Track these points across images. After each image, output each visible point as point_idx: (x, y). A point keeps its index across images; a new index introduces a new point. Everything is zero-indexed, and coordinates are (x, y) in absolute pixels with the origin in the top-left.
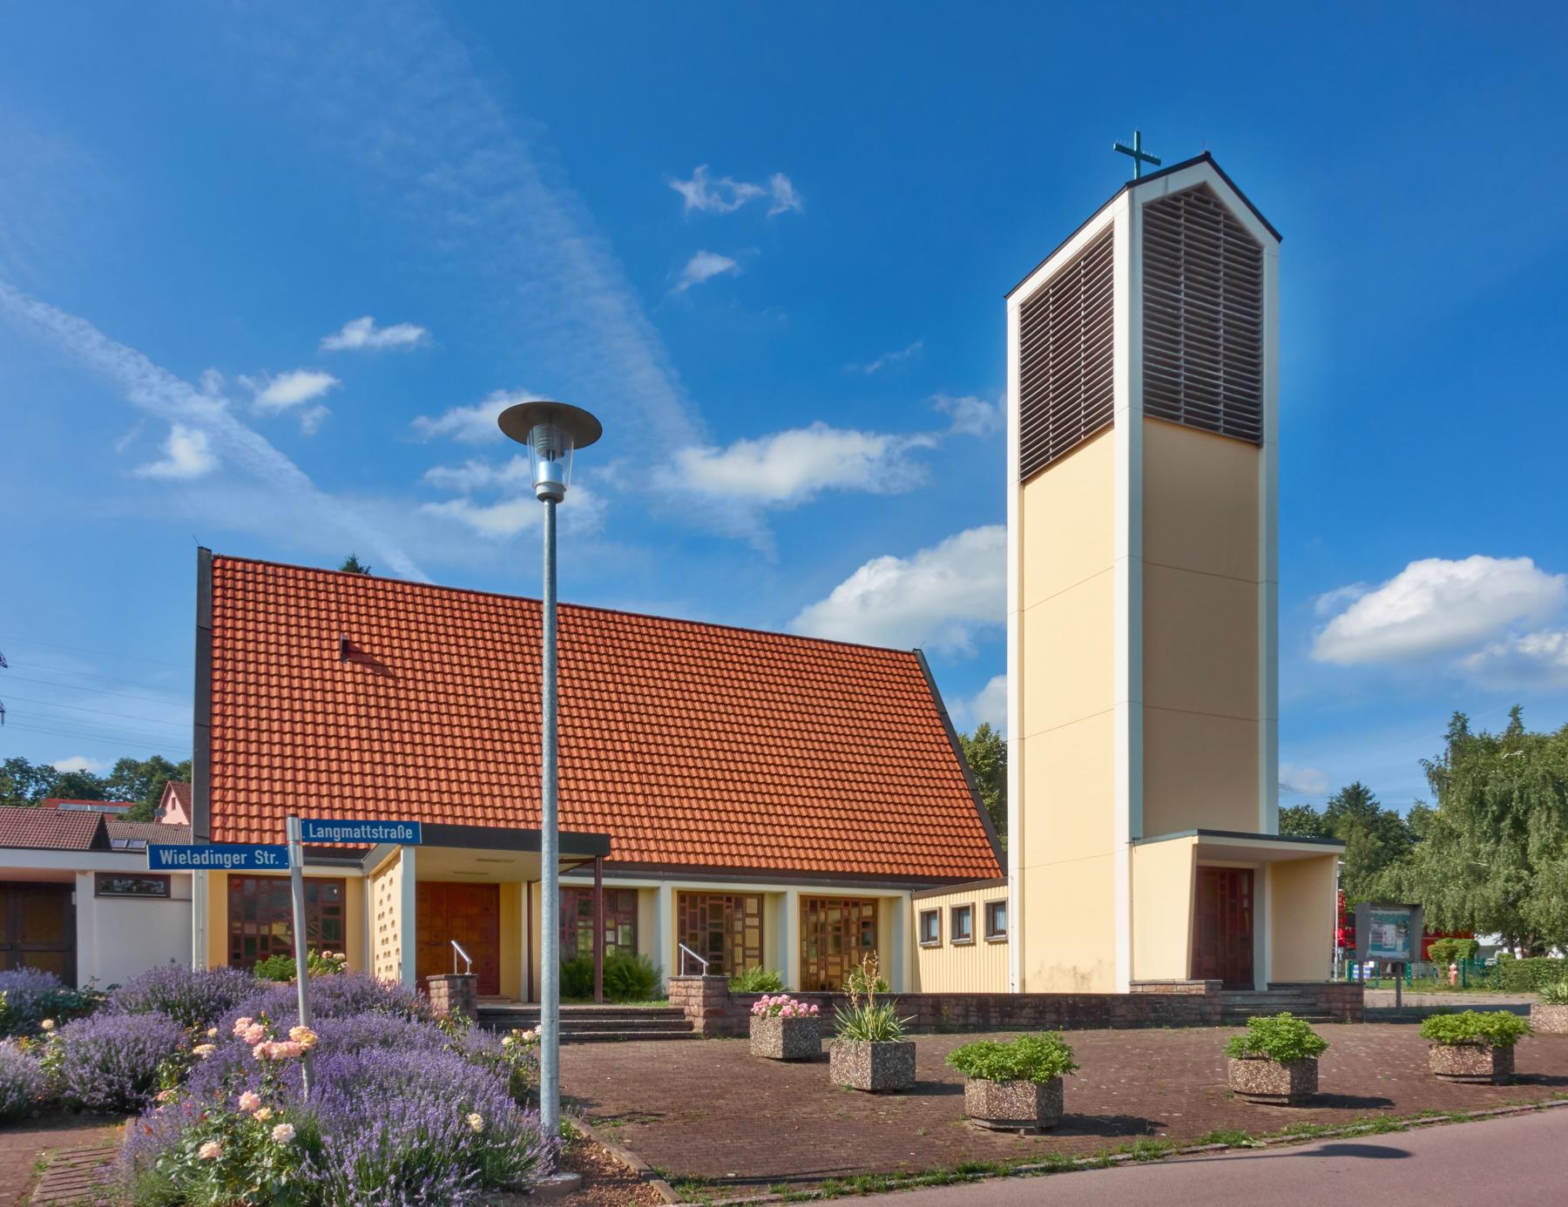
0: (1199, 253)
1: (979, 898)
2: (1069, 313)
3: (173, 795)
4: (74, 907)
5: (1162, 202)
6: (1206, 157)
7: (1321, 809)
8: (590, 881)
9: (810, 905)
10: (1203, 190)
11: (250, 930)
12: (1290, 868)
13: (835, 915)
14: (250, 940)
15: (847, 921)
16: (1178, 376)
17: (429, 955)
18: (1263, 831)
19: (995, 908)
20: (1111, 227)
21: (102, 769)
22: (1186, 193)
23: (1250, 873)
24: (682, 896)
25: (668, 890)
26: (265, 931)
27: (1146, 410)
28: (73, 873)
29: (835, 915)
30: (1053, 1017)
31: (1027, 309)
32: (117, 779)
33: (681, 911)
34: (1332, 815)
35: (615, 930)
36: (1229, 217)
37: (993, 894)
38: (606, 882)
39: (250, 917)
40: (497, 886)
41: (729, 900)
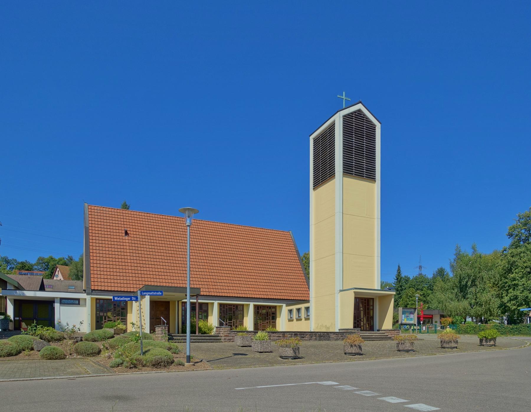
0: (358, 131)
1: (303, 306)
2: (325, 142)
3: (58, 269)
4: (54, 308)
5: (348, 115)
6: (361, 102)
7: (430, 276)
8: (195, 301)
9: (257, 308)
10: (359, 110)
11: (101, 314)
12: (382, 298)
13: (264, 311)
14: (101, 317)
15: (511, 300)
16: (352, 162)
17: (155, 322)
18: (376, 288)
19: (307, 309)
20: (334, 121)
21: (33, 261)
22: (355, 112)
23: (373, 299)
24: (221, 305)
25: (216, 303)
26: (105, 314)
27: (344, 172)
28: (54, 298)
29: (264, 311)
30: (315, 338)
31: (316, 141)
32: (38, 263)
33: (220, 309)
34: (434, 277)
35: (202, 315)
36: (367, 118)
37: (306, 305)
38: (199, 301)
39: (101, 311)
40: (169, 302)
41: (234, 306)
